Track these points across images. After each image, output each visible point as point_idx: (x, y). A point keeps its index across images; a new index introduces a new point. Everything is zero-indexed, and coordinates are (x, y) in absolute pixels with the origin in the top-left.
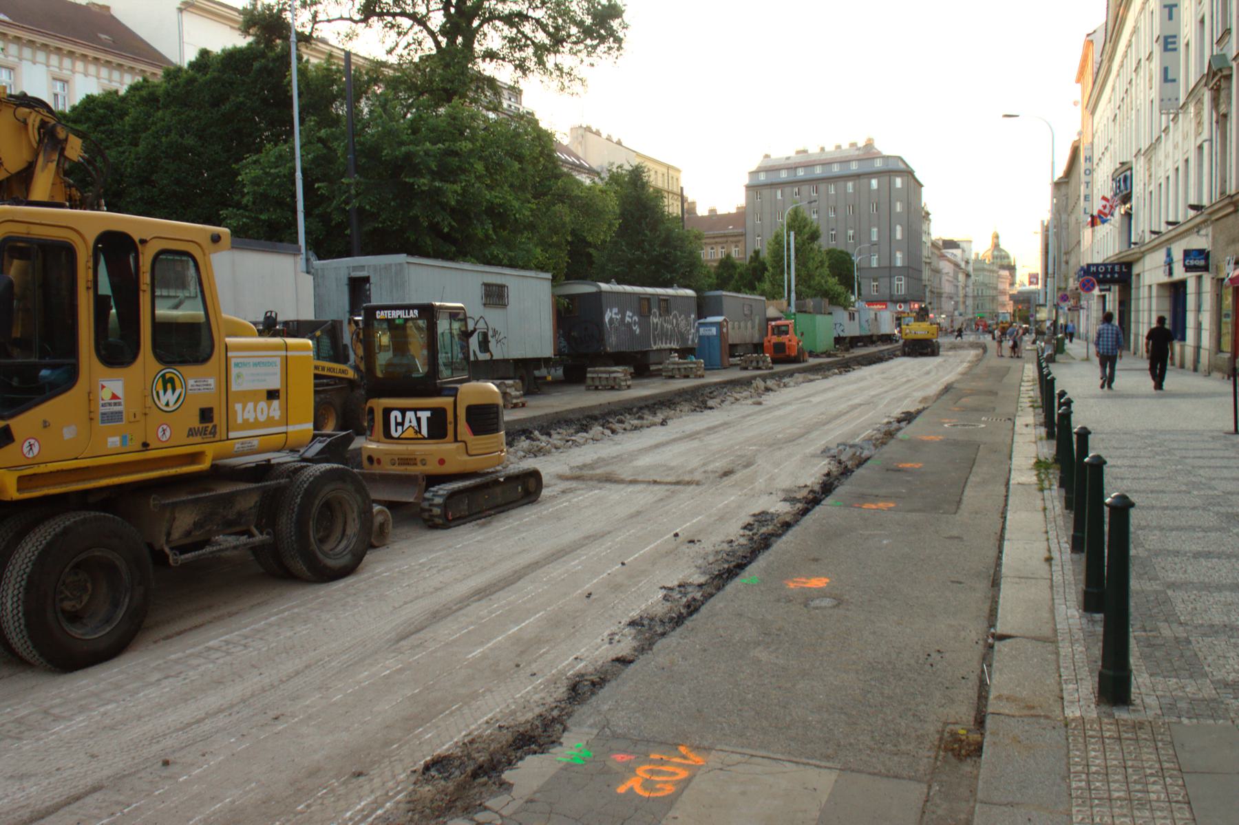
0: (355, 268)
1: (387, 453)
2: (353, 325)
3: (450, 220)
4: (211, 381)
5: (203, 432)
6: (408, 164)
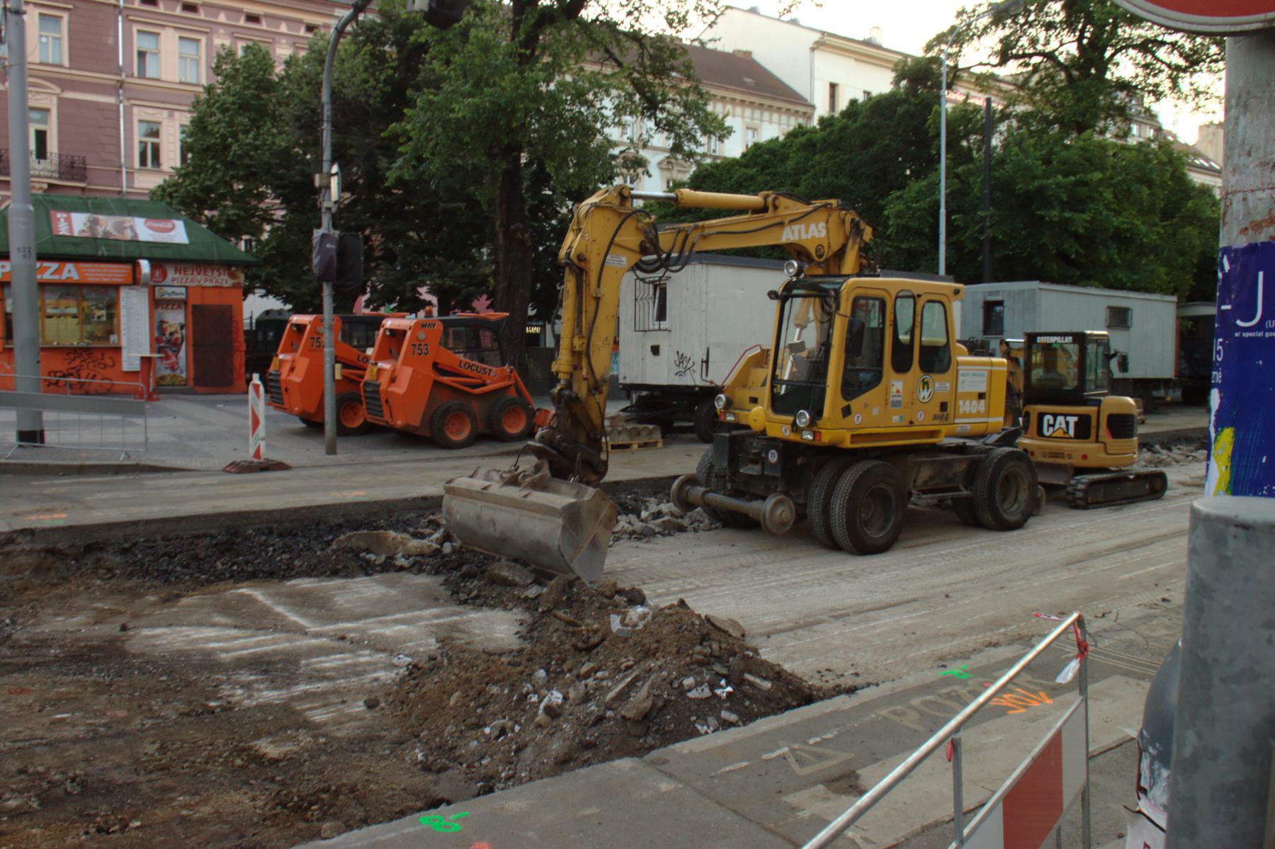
0: (990, 293)
1: (1040, 447)
2: (1004, 345)
3: (1077, 247)
4: (948, 385)
5: (941, 418)
6: (1041, 197)
